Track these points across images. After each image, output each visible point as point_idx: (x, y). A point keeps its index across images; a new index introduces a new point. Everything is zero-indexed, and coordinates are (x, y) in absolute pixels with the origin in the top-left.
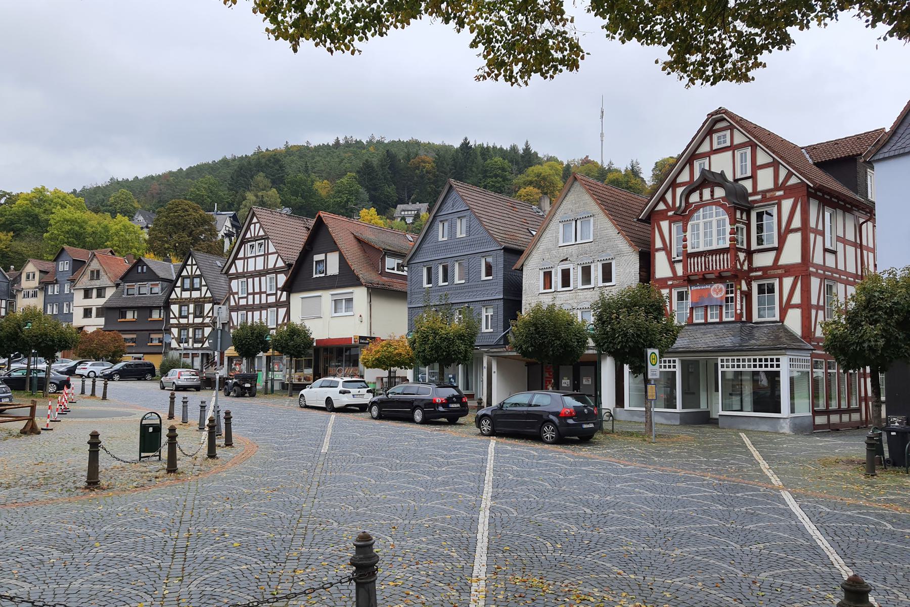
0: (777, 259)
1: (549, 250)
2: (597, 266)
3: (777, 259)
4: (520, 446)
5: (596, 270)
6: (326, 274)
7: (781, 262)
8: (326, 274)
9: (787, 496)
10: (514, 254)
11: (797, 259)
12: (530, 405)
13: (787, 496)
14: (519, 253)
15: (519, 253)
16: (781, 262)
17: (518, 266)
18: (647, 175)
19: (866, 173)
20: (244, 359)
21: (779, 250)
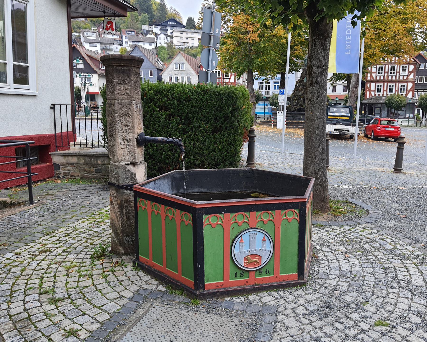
0: (229, 81)
1: (171, 71)
2: (186, 77)
3: (229, 81)
4: (7, 211)
5: (186, 78)
6: (77, 67)
7: (230, 81)
8: (77, 67)
9: (292, 274)
10: (160, 70)
11: (233, 81)
12: (155, 181)
13: (292, 274)
14: (162, 70)
15: (162, 70)
16: (230, 81)
17: (161, 74)
18: (287, 106)
19: (159, 25)
20: (177, 291)
21: (230, 79)
